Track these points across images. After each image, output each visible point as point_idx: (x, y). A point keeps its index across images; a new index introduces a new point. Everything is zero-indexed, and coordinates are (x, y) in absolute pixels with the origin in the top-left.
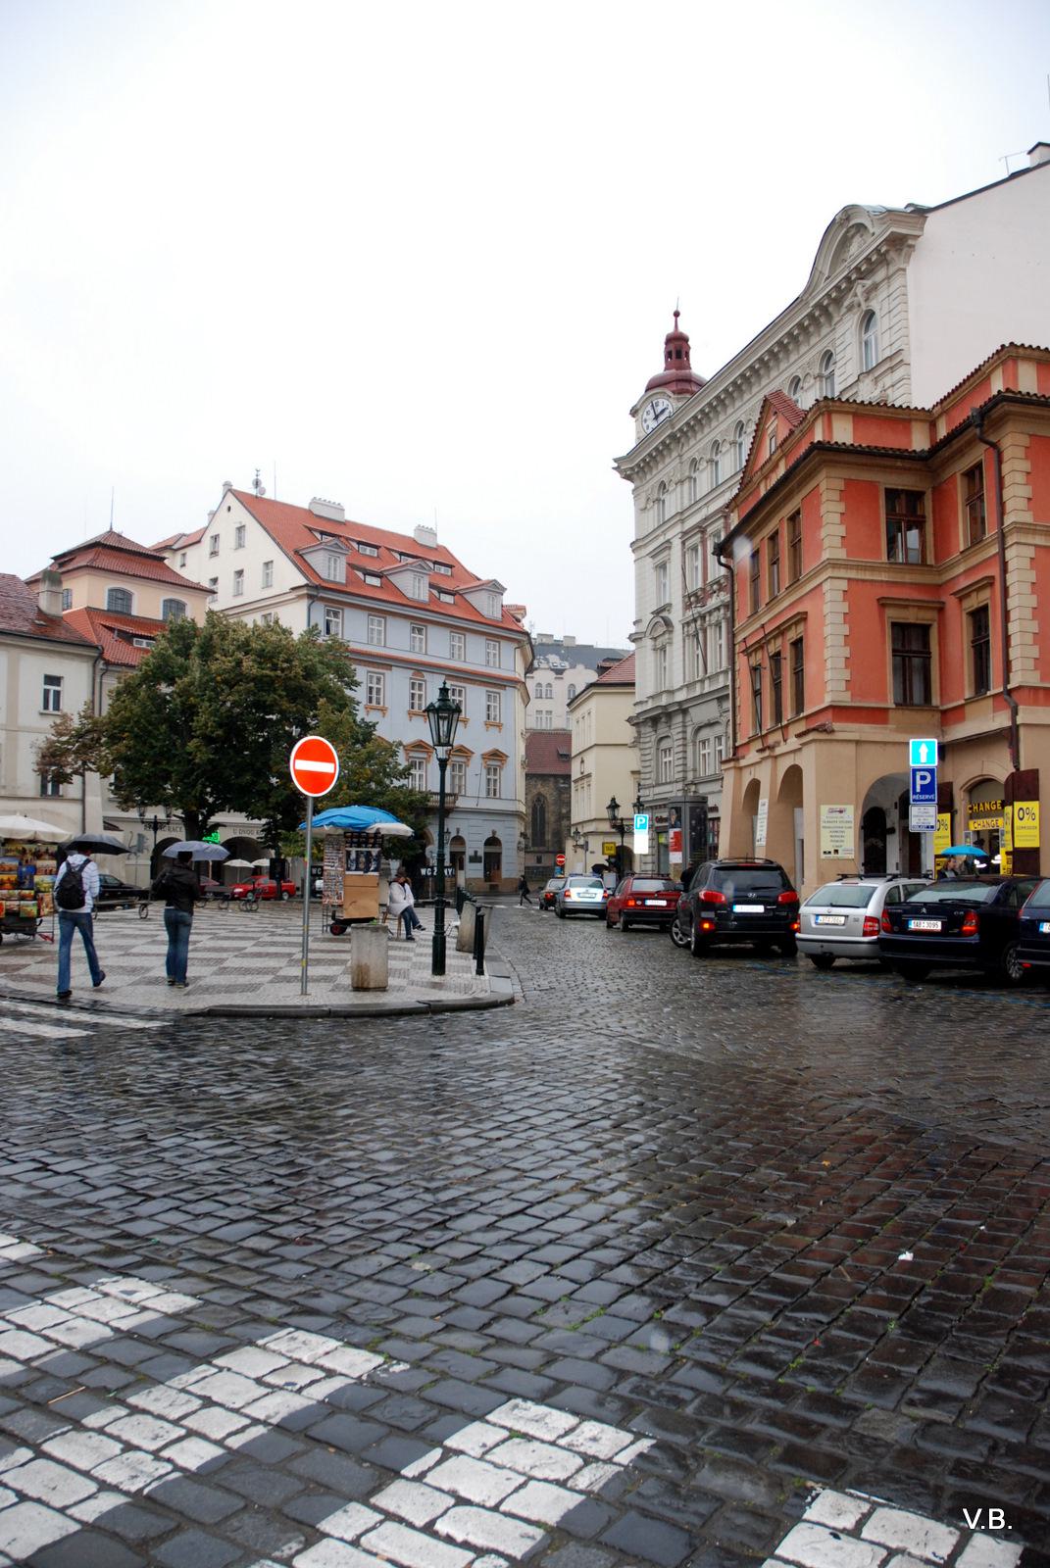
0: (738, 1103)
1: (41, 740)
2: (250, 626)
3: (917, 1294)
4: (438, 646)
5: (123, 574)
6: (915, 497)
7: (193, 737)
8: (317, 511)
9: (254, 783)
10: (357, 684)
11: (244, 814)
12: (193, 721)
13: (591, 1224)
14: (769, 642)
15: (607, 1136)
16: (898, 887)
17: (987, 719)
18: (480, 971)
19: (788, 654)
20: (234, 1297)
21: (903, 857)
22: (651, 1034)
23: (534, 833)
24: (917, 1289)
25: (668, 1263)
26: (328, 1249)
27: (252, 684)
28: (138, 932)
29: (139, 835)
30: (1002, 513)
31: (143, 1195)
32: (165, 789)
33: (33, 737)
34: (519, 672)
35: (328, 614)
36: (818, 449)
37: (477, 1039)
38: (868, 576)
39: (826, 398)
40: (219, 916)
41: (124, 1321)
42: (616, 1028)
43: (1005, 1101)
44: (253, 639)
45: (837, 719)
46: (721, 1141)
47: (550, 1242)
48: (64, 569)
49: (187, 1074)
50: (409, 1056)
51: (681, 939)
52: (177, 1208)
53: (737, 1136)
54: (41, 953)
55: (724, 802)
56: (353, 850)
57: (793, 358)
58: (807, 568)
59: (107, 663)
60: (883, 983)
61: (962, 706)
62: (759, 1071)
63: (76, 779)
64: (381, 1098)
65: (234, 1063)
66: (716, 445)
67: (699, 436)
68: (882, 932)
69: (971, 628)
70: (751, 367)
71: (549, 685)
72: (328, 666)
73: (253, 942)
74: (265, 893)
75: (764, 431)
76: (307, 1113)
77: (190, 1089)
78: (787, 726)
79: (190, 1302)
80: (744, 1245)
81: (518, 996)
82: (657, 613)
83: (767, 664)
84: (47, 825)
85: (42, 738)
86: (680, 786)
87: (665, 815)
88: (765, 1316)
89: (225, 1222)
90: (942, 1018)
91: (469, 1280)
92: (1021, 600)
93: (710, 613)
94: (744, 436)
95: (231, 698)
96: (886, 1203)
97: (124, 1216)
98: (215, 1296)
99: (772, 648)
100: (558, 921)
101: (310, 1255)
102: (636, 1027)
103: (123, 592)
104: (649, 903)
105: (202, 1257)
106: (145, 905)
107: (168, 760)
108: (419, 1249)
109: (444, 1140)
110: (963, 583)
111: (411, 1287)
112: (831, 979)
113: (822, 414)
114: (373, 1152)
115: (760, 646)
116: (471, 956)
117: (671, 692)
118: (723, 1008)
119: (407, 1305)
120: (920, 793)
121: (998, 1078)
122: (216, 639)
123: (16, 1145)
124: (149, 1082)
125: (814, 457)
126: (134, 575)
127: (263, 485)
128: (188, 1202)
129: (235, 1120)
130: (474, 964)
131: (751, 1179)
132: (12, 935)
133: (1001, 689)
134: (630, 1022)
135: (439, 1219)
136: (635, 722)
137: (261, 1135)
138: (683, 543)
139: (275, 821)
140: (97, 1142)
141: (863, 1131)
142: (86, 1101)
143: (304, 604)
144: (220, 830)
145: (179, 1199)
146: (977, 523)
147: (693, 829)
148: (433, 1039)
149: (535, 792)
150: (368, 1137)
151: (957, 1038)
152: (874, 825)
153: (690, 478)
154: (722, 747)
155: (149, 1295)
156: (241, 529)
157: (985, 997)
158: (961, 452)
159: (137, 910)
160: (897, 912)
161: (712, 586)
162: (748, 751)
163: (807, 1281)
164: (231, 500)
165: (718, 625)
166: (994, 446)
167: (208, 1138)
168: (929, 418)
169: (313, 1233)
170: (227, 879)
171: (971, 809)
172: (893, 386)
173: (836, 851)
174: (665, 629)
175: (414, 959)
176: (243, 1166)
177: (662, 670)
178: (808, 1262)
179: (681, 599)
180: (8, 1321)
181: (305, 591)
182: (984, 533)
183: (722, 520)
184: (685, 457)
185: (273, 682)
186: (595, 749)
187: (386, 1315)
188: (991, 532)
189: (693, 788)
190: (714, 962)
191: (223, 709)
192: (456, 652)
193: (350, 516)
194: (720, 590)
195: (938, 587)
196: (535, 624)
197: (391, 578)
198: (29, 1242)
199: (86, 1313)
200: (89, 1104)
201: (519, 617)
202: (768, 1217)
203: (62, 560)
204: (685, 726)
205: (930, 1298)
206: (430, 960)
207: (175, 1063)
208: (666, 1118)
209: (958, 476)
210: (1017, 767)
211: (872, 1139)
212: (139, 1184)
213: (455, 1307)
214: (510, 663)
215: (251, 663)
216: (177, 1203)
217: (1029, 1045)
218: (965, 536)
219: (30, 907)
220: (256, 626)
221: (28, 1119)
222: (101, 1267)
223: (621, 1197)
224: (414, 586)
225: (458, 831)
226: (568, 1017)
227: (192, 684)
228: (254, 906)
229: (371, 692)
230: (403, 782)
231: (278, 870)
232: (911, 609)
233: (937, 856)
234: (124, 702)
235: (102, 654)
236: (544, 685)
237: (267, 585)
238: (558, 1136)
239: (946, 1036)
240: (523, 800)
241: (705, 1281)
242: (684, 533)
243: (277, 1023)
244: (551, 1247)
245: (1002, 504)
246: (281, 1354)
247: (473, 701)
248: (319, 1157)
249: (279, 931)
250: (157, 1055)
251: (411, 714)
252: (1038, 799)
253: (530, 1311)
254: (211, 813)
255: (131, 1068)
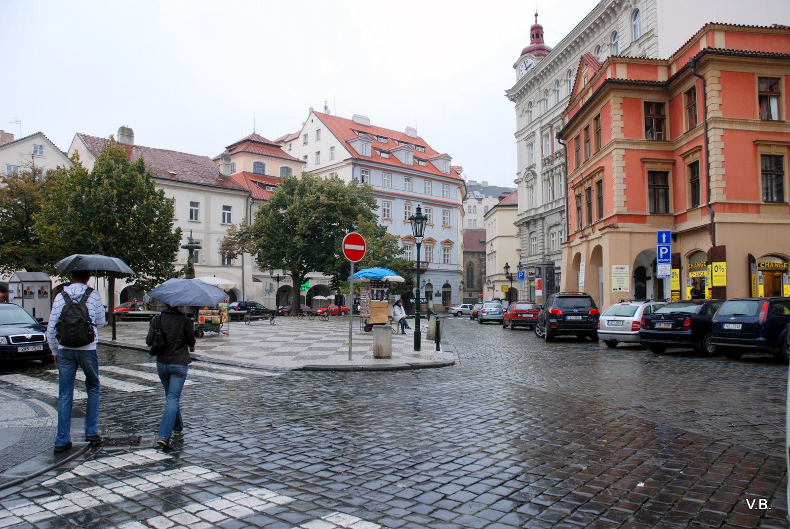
0: (562, 412)
1: (221, 238)
2: (324, 179)
3: (645, 502)
4: (418, 188)
5: (261, 155)
6: (660, 106)
7: (296, 235)
8: (356, 121)
9: (327, 257)
10: (377, 207)
11: (322, 273)
12: (296, 227)
13: (486, 467)
14: (585, 182)
15: (497, 427)
16: (650, 306)
17: (699, 220)
18: (438, 349)
19: (594, 188)
20: (310, 498)
21: (655, 292)
22: (521, 379)
23: (468, 282)
24: (645, 500)
25: (522, 486)
26: (357, 477)
27: (325, 208)
28: (269, 331)
29: (270, 284)
30: (706, 112)
31: (270, 452)
32: (282, 261)
33: (218, 236)
34: (459, 200)
35: (363, 172)
36: (610, 82)
37: (435, 381)
38: (635, 147)
39: (612, 56)
40: (309, 324)
41: (259, 507)
42: (504, 376)
43: (699, 412)
44: (325, 185)
45: (619, 221)
46: (554, 430)
47: (465, 475)
48: (232, 153)
49: (292, 397)
50: (401, 389)
51: (540, 334)
52: (285, 458)
53: (561, 427)
54: (222, 341)
55: (563, 263)
56: (375, 290)
57: (596, 35)
58: (604, 143)
59: (254, 199)
60: (643, 355)
61: (685, 213)
62: (575, 397)
63: (239, 256)
64: (386, 409)
65: (314, 392)
66: (557, 82)
67: (549, 78)
68: (641, 329)
69: (690, 173)
70: (575, 41)
71: (475, 206)
72: (363, 198)
73: (325, 335)
74: (333, 312)
75: (581, 74)
76: (349, 415)
77: (293, 404)
78: (594, 225)
79: (290, 500)
80: (559, 478)
81: (457, 361)
82: (528, 169)
83: (584, 193)
84: (221, 280)
85: (222, 236)
86: (541, 257)
87: (533, 272)
88: (568, 511)
89: (309, 464)
90: (670, 372)
91: (424, 492)
92: (716, 158)
93: (556, 168)
94: (571, 77)
95: (314, 215)
96: (633, 460)
97: (261, 461)
98: (302, 497)
99: (586, 186)
100: (479, 325)
101: (348, 480)
102: (515, 376)
103: (261, 164)
104: (524, 316)
105: (297, 480)
106: (273, 318)
107: (284, 246)
108: (401, 478)
109: (417, 428)
110: (686, 150)
111: (396, 495)
112: (615, 353)
113: (611, 64)
114: (381, 433)
115: (581, 184)
116: (434, 342)
117: (536, 209)
118: (559, 367)
119: (393, 503)
120: (662, 258)
121: (697, 401)
122: (307, 186)
123: (209, 429)
124: (273, 401)
125: (607, 87)
126: (266, 155)
127: (329, 108)
128: (291, 455)
129: (314, 419)
130: (435, 345)
131: (567, 447)
132: (209, 332)
133: (705, 204)
134: (512, 373)
135: (412, 464)
136: (518, 224)
137: (327, 425)
138: (541, 133)
139: (337, 276)
140: (248, 427)
141: (626, 426)
142: (243, 409)
143: (350, 167)
144: (310, 281)
145: (287, 454)
146: (693, 118)
147: (547, 278)
148: (413, 382)
149: (468, 261)
150: (379, 427)
151: (678, 382)
152: (640, 275)
153: (544, 99)
154: (562, 237)
155: (272, 496)
156: (318, 131)
157: (693, 362)
158: (684, 82)
159: (269, 320)
160: (649, 319)
161: (556, 154)
162: (575, 238)
163: (590, 495)
164: (313, 117)
165: (560, 174)
166: (701, 77)
167: (301, 426)
168: (667, 64)
169: (351, 469)
170: (314, 304)
171: (690, 266)
172: (649, 48)
173: (620, 289)
174: (532, 177)
175: (405, 343)
176: (318, 439)
177: (531, 198)
178: (591, 486)
179: (540, 161)
180: (206, 506)
181: (350, 161)
182: (696, 123)
183: (561, 121)
184: (542, 89)
185: (335, 206)
186: (498, 239)
187: (382, 507)
188: (700, 122)
189: (548, 258)
190: (557, 345)
191: (311, 221)
192: (427, 190)
193: (373, 123)
194: (560, 156)
195: (672, 152)
196: (467, 176)
197: (394, 154)
198: (216, 472)
199: (241, 503)
200: (244, 411)
201: (459, 172)
202: (574, 465)
203: (230, 148)
204: (543, 226)
205: (651, 504)
206: (413, 344)
207: (286, 392)
208: (526, 419)
209: (683, 93)
210: (714, 245)
211: (630, 430)
212: (267, 447)
213: (417, 504)
214: (454, 195)
215: (324, 198)
216: (286, 456)
217: (716, 385)
218: (686, 124)
219: (217, 319)
220: (326, 179)
221: (215, 417)
222: (249, 483)
223: (501, 455)
224: (406, 158)
225: (429, 280)
226: (481, 371)
227: (295, 208)
228: (327, 319)
229: (384, 212)
230: (401, 256)
231: (339, 301)
232: (658, 164)
233: (672, 291)
234: (262, 218)
235: (251, 194)
236: (472, 207)
237: (332, 159)
238: (471, 427)
239: (672, 381)
240: (462, 265)
241: (539, 494)
242: (542, 128)
243: (336, 374)
244: (465, 478)
245: (706, 108)
246: (332, 523)
247: (436, 215)
248: (355, 435)
249: (339, 330)
250: (277, 388)
251: (405, 222)
252: (725, 261)
253: (453, 507)
254: (305, 273)
255: (265, 394)
